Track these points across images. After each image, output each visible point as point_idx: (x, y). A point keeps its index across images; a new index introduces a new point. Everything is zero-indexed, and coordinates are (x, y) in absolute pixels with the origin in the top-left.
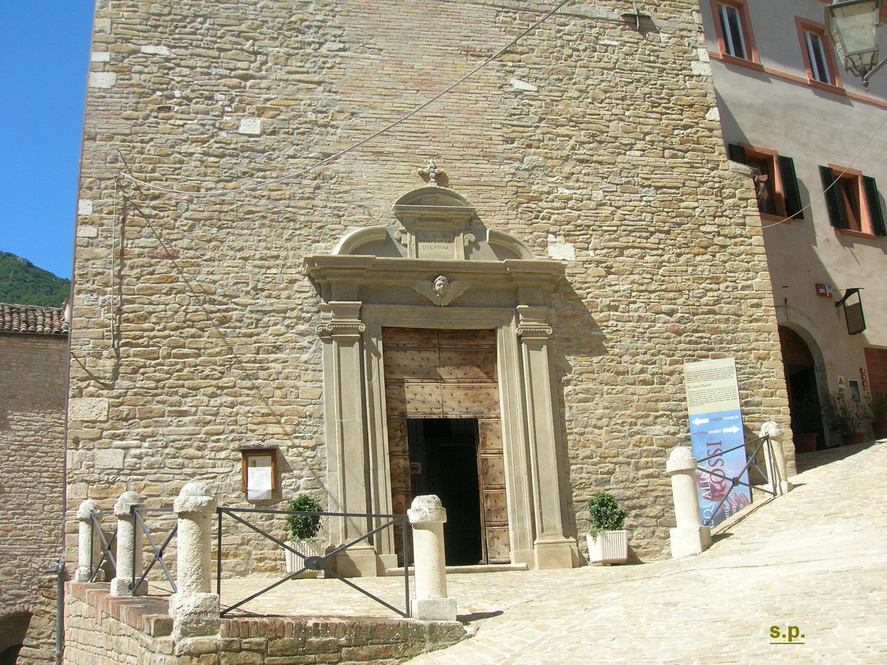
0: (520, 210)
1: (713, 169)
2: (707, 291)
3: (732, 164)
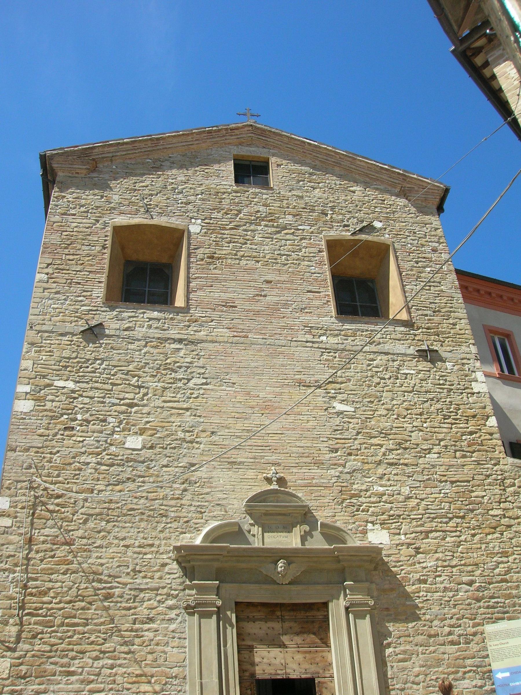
0: (344, 505)
1: (495, 465)
2: (499, 563)
3: (510, 460)
